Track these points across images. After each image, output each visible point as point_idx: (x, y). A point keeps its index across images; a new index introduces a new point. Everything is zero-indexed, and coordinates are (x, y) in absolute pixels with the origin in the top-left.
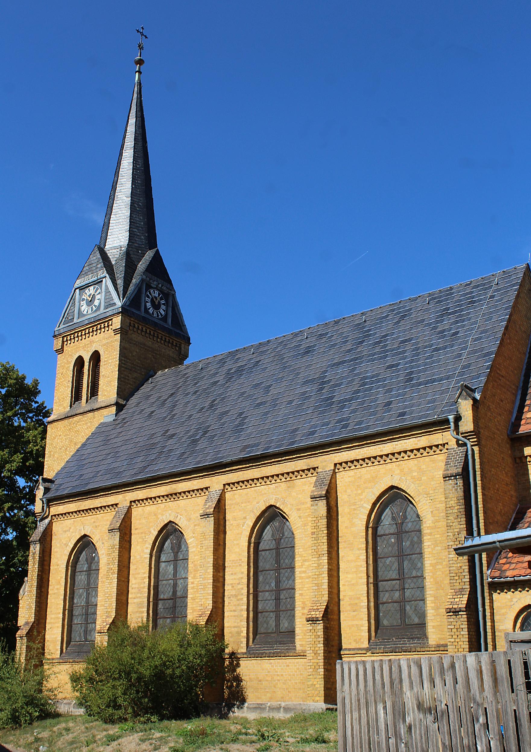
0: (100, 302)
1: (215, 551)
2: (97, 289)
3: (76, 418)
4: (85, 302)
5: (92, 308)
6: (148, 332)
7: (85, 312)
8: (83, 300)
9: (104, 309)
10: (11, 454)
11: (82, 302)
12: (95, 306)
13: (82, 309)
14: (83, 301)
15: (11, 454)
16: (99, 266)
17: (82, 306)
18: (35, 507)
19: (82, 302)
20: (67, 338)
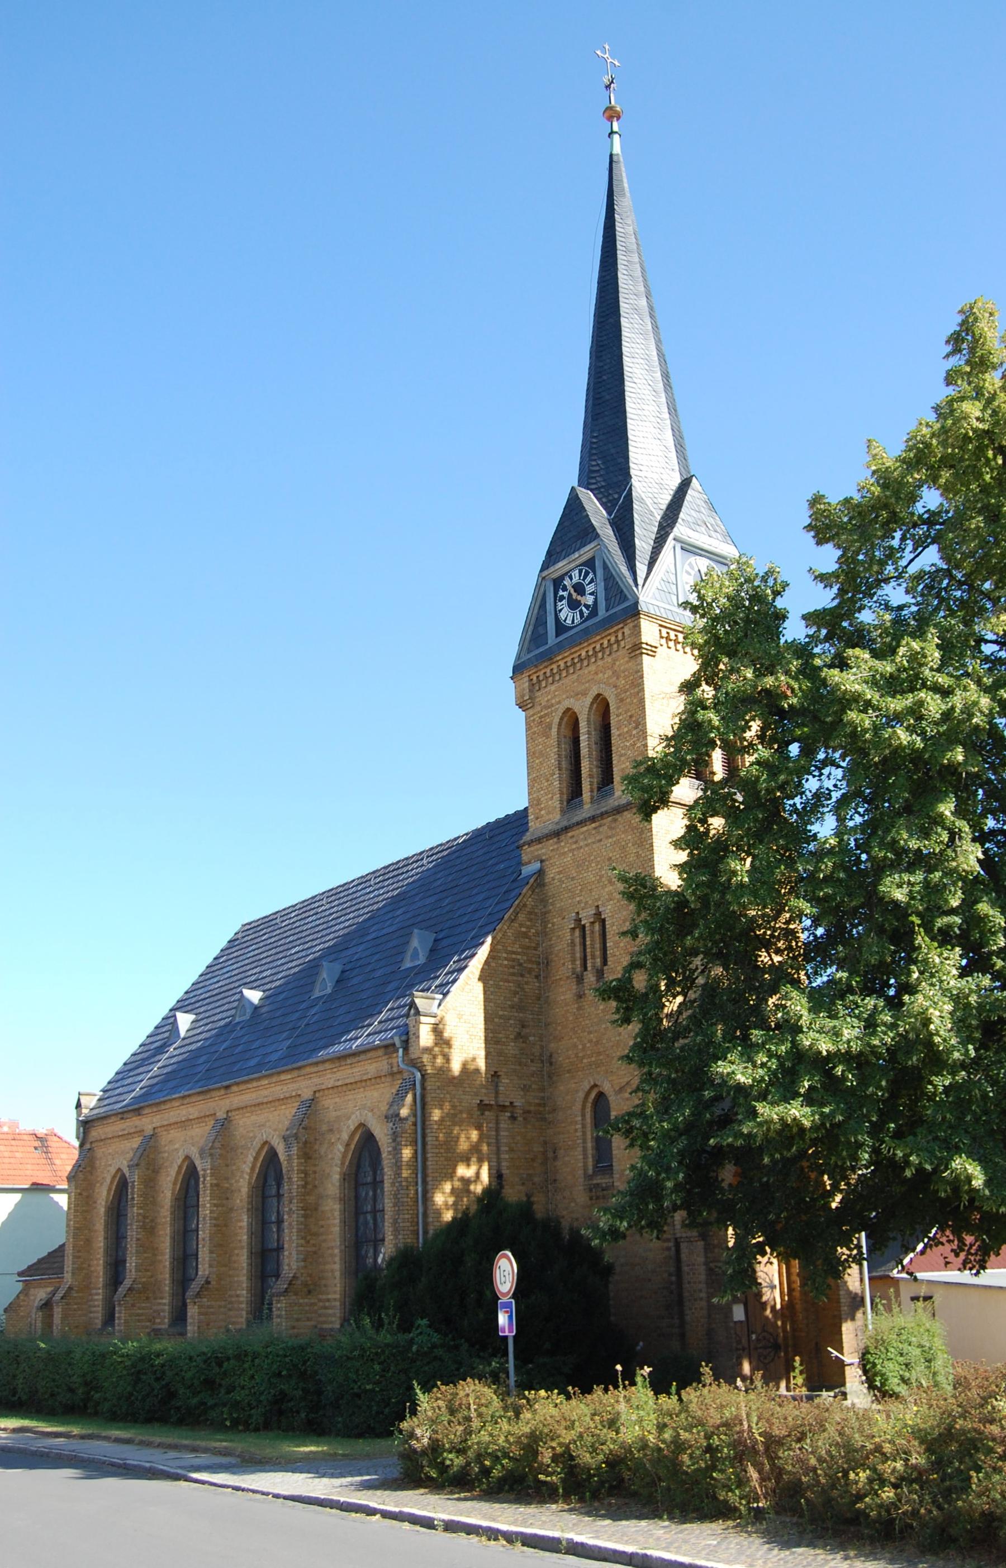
0: (596, 599)
1: (605, 1560)
2: (587, 574)
3: (206, 1486)
4: (564, 602)
5: (581, 612)
6: (664, 635)
7: (569, 621)
8: (562, 598)
9: (557, 636)
10: (820, 669)
11: (559, 604)
12: (587, 606)
13: (562, 616)
14: (560, 601)
15: (820, 669)
16: (973, 409)
17: (560, 611)
18: (943, 393)
19: (559, 604)
20: (602, 644)
